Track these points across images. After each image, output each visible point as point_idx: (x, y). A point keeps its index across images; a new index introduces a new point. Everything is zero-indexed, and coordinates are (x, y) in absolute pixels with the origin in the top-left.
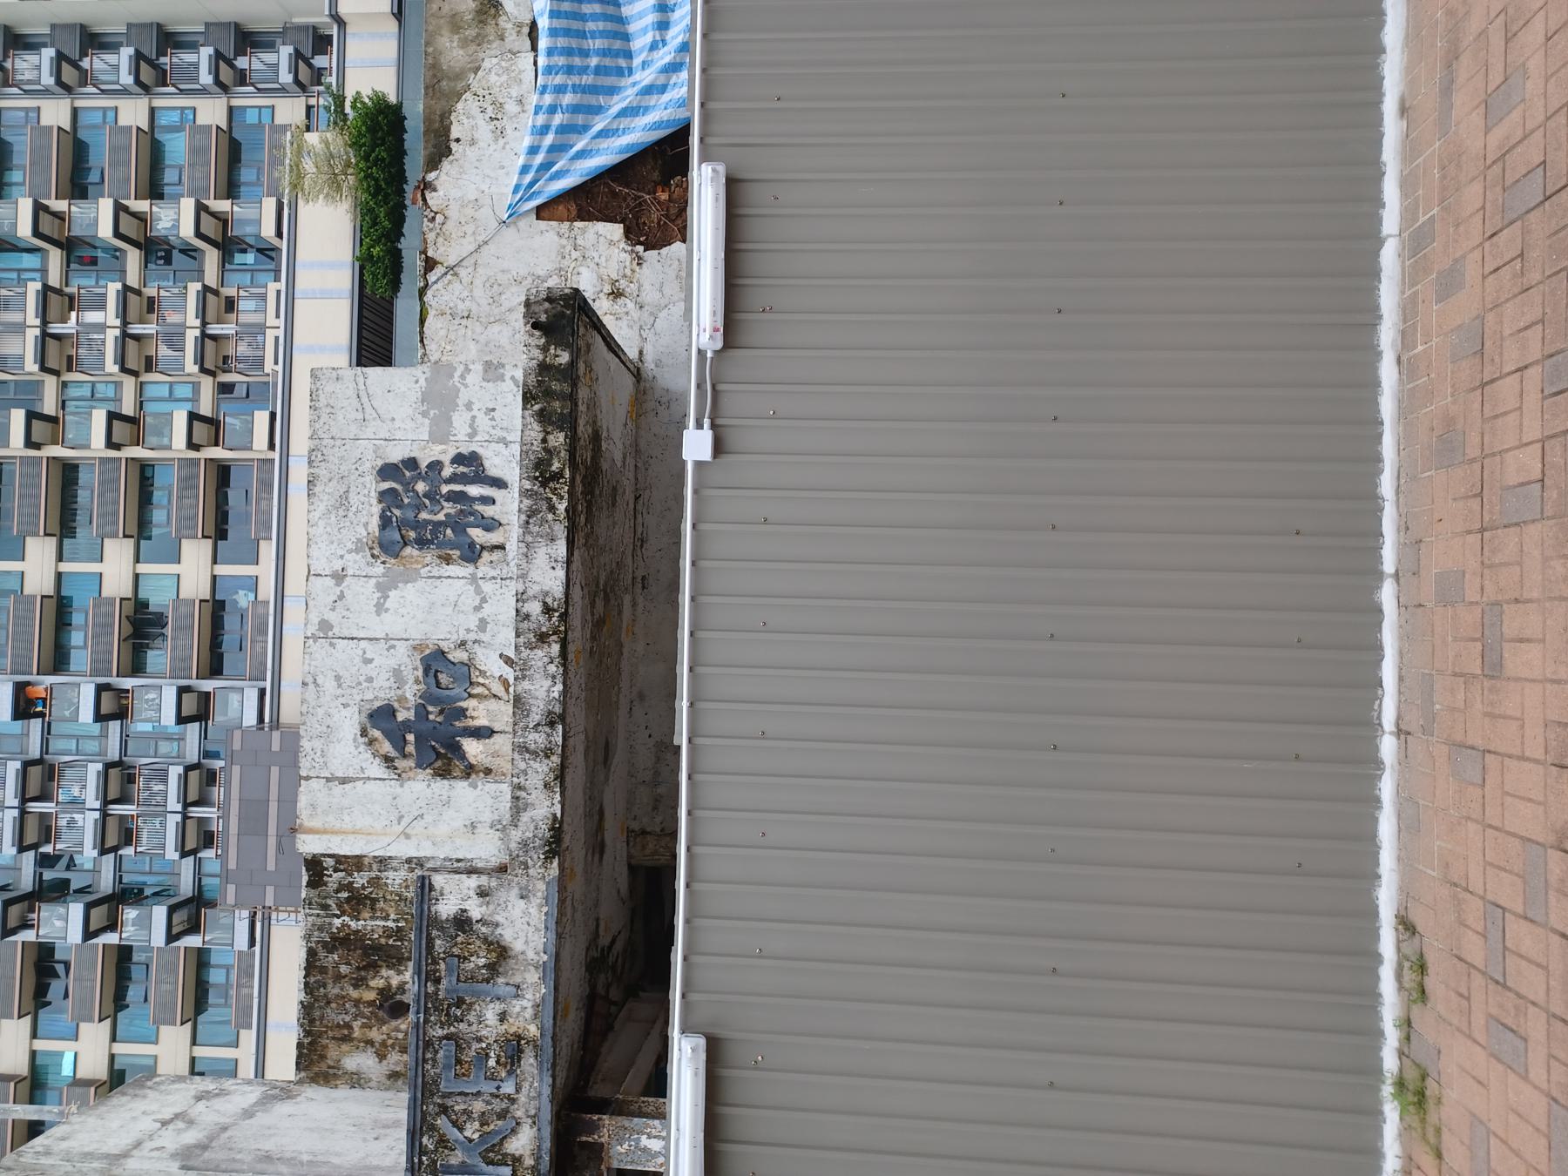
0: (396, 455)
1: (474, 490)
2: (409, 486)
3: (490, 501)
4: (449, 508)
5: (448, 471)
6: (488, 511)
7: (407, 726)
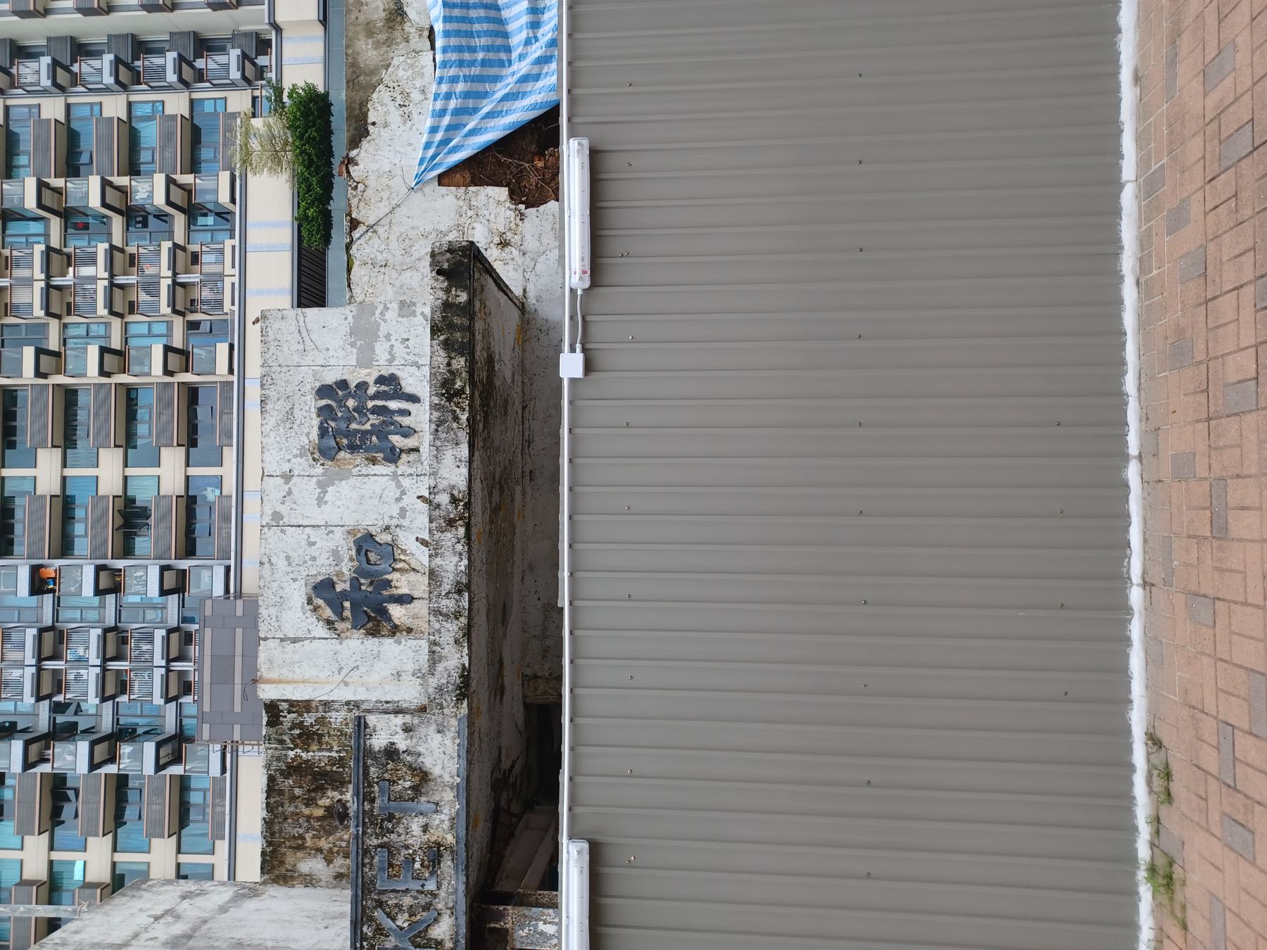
0: (330, 378)
1: (394, 405)
3: (407, 413)
4: (374, 419)
5: (372, 390)
6: (405, 421)
7: (344, 595)
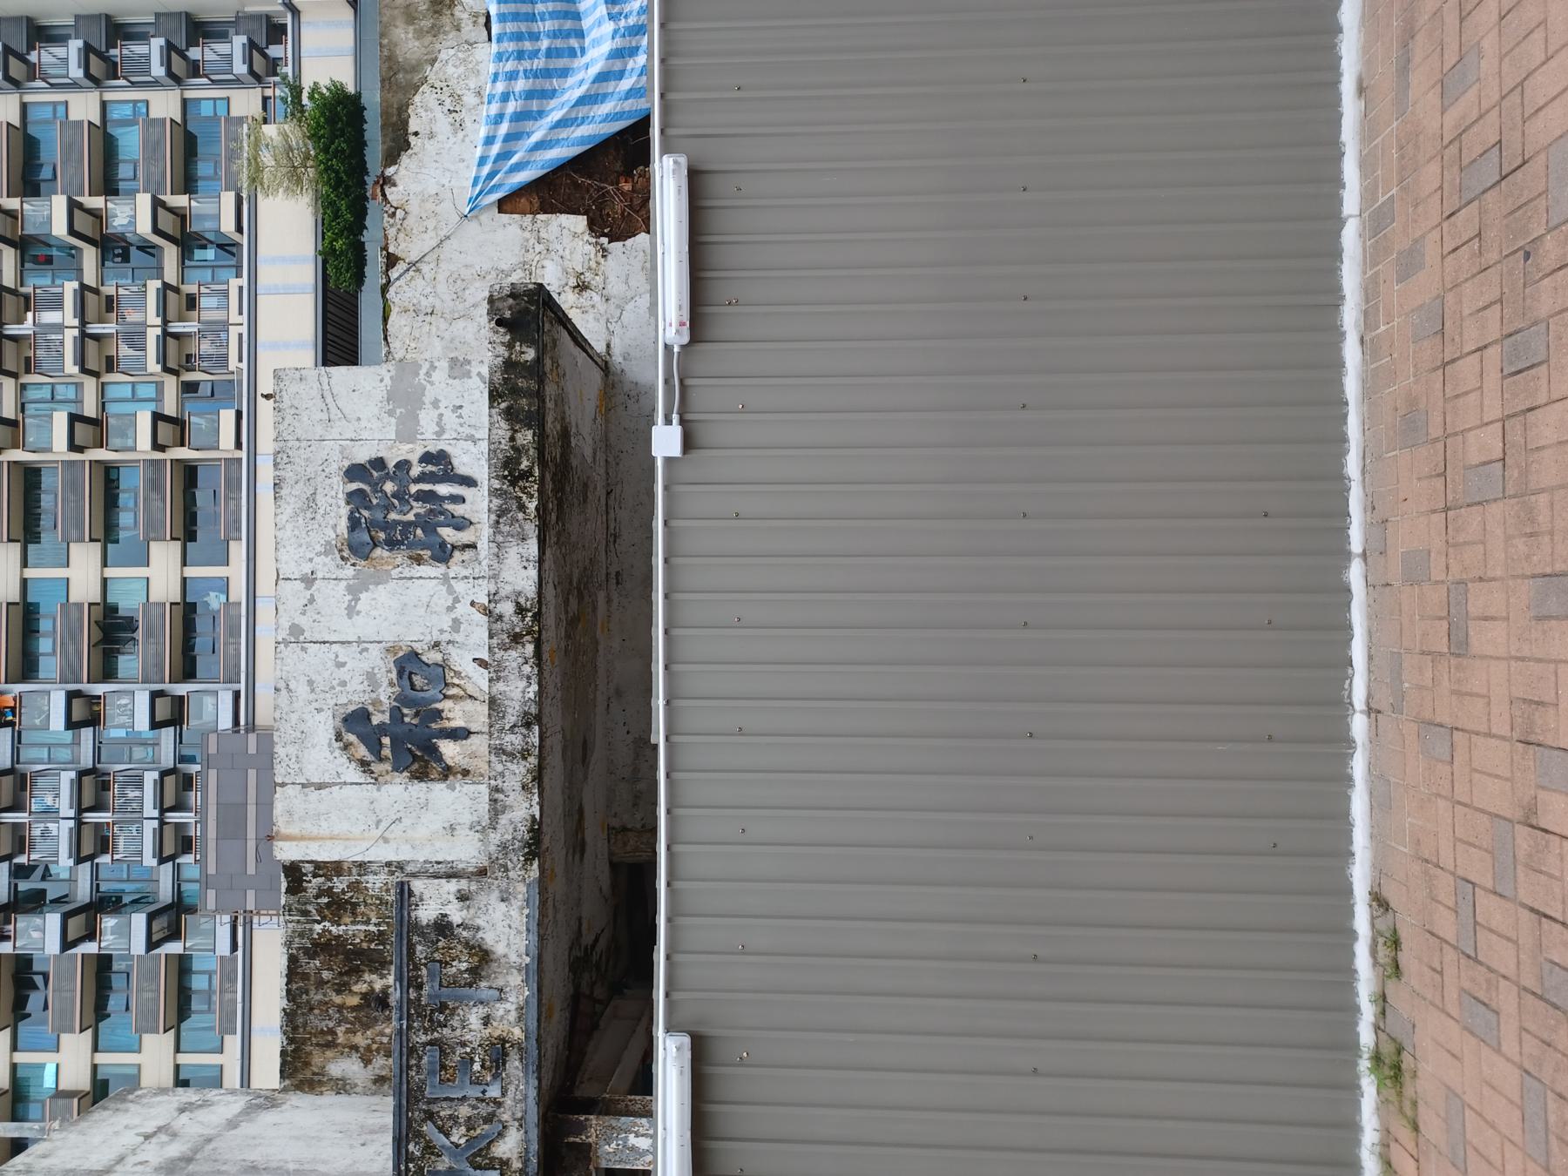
0: (363, 455)
1: (443, 489)
2: (377, 486)
4: (419, 508)
5: (416, 471)
6: (458, 510)
7: (382, 729)
